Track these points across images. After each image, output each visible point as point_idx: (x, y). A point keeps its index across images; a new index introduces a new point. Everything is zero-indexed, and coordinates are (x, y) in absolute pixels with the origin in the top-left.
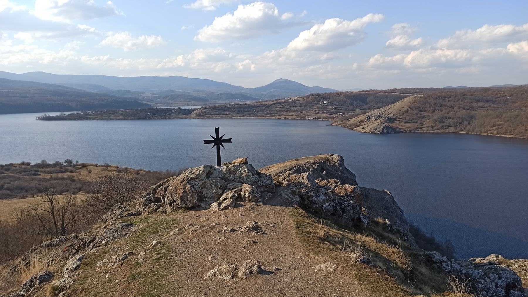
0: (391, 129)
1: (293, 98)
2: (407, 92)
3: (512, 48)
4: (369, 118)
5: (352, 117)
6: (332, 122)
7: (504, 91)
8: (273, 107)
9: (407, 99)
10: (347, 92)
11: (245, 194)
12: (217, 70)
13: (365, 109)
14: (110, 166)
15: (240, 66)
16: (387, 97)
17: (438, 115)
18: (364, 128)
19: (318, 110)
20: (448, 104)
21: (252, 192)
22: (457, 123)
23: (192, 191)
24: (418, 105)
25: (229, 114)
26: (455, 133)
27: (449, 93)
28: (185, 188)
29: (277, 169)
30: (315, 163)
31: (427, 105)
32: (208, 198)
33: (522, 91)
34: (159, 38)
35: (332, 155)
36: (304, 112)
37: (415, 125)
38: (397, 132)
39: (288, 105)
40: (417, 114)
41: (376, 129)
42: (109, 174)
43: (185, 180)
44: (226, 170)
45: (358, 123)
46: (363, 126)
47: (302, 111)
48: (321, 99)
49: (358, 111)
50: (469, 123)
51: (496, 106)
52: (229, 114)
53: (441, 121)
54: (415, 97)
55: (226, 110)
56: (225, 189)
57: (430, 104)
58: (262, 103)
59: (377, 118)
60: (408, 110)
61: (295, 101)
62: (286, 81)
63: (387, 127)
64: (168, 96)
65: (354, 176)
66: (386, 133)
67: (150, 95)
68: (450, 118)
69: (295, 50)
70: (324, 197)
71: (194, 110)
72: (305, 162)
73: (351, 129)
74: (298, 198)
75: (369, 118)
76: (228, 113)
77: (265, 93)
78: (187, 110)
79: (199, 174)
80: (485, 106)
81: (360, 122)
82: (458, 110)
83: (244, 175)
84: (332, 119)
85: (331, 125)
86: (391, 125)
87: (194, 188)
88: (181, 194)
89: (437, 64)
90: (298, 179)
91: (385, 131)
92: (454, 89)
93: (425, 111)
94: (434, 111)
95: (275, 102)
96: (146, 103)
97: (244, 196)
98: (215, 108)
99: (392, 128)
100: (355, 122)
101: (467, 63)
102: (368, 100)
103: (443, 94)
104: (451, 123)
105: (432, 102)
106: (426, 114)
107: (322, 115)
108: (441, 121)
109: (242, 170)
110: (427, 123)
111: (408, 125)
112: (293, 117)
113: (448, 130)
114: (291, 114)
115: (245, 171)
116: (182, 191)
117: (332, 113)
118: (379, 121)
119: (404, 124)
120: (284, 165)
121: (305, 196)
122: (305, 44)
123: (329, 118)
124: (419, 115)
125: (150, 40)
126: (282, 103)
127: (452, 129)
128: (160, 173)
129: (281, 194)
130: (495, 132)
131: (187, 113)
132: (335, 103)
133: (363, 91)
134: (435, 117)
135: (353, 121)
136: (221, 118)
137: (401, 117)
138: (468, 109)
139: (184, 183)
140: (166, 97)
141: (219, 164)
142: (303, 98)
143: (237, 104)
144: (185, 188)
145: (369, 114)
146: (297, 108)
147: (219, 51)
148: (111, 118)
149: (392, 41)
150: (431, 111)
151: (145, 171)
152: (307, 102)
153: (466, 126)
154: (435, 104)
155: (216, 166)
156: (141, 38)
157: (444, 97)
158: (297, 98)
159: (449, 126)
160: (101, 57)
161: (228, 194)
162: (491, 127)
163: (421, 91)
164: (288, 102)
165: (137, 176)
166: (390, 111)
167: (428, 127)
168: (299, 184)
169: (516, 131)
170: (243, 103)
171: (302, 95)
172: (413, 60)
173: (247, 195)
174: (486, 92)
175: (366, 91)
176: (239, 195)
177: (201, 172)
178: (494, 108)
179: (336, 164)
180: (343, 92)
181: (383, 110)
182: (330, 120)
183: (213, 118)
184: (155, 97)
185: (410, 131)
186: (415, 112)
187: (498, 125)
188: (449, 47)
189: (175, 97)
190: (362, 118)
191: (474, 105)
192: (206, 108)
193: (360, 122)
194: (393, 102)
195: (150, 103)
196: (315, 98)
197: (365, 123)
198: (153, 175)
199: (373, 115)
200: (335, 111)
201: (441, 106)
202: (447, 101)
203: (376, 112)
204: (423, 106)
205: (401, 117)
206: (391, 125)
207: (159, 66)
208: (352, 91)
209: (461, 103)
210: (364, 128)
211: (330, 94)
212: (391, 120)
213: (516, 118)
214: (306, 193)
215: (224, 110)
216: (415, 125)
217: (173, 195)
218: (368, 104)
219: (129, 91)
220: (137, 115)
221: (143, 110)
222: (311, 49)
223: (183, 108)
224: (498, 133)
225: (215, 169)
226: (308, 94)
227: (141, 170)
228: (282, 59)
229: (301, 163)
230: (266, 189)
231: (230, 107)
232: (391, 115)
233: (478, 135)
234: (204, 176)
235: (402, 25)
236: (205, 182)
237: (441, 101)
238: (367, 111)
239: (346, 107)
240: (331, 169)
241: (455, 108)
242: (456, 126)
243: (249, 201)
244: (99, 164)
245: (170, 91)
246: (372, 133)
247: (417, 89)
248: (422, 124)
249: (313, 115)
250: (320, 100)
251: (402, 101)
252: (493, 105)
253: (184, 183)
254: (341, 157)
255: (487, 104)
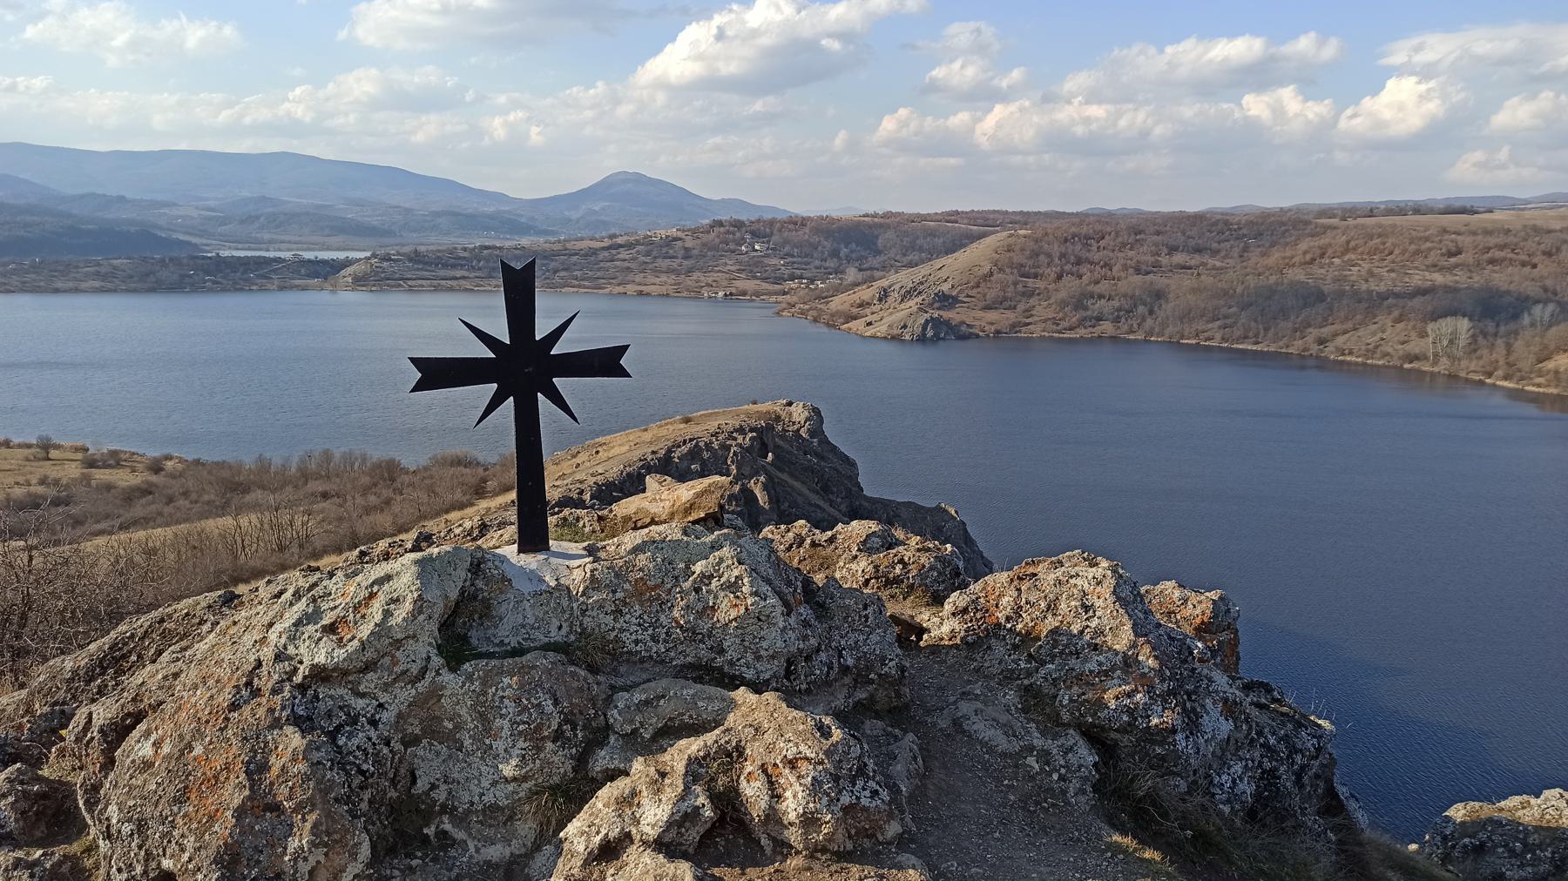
0: (945, 328)
1: (663, 233)
2: (987, 222)
3: (1255, 105)
4: (884, 295)
5: (838, 290)
6: (779, 307)
7: (1238, 223)
8: (601, 257)
9: (988, 240)
10: (821, 218)
11: (776, 796)
12: (420, 137)
13: (871, 269)
14: (57, 447)
15: (497, 127)
16: (932, 234)
17: (1070, 286)
18: (870, 324)
19: (739, 271)
20: (1097, 257)
21: (836, 777)
22: (1119, 310)
23: (324, 789)
24: (1017, 258)
25: (463, 278)
26: (1113, 338)
27: (1098, 227)
28: (256, 769)
29: (625, 448)
30: (741, 430)
31: (1042, 257)
32: (461, 820)
33: (1283, 224)
34: (228, 31)
35: (790, 404)
36: (696, 275)
37: (1011, 316)
38: (962, 334)
39: (648, 254)
40: (1015, 284)
41: (905, 327)
42: (53, 472)
43: (265, 682)
44: (594, 583)
45: (855, 310)
46: (868, 319)
47: (690, 271)
48: (748, 236)
49: (852, 274)
50: (1151, 312)
51: (1218, 264)
52: (463, 278)
53: (1079, 305)
54: (1011, 236)
55: (454, 266)
56: (599, 736)
57: (1049, 255)
58: (568, 246)
59: (907, 295)
60: (991, 274)
61: (670, 241)
62: (639, 179)
63: (936, 323)
64: (258, 217)
65: (853, 464)
66: (931, 339)
67: (195, 213)
68: (1101, 297)
69: (661, 84)
70: (1226, 727)
71: (347, 263)
72: (712, 426)
73: (834, 326)
74: (1086, 756)
75: (884, 295)
76: (459, 273)
77: (574, 215)
78: (324, 262)
79: (382, 629)
80: (1193, 263)
81: (860, 306)
82: (1123, 275)
83: (727, 611)
84: (780, 298)
85: (778, 313)
86: (946, 315)
87: (341, 760)
88: (224, 828)
89: (1058, 142)
90: (1052, 607)
91: (930, 333)
92: (1110, 214)
93: (1036, 276)
94: (1060, 277)
95: (607, 243)
96: (182, 237)
97: (773, 817)
98: (416, 258)
99: (947, 323)
100: (846, 307)
101: (1140, 143)
102: (880, 242)
103: (1084, 230)
104: (1106, 311)
105: (1056, 249)
106: (1040, 284)
107: (750, 285)
108: (1079, 305)
109: (707, 578)
110: (1042, 310)
111: (992, 315)
112: (663, 290)
113: (1098, 330)
114: (657, 280)
115: (733, 587)
116: (233, 794)
117: (778, 280)
118: (913, 304)
119: (980, 314)
120: (647, 436)
121: (1123, 730)
122: (693, 69)
123: (770, 294)
124: (1020, 287)
125: (195, 35)
126: (629, 246)
127: (1107, 327)
128: (237, 468)
129: (957, 723)
130: (1218, 336)
131: (326, 272)
132: (787, 248)
133: (866, 215)
134: (1063, 294)
135: (839, 303)
136: (437, 289)
137: (973, 292)
138: (1148, 273)
139: (254, 713)
140: (249, 219)
141: (533, 538)
142: (694, 231)
143: (487, 248)
144: (256, 769)
145: (884, 283)
146: (675, 264)
147: (426, 76)
148: (59, 285)
149: (938, 73)
150: (1053, 276)
151: (181, 460)
152: (704, 245)
153: (1144, 319)
154: (1063, 256)
155: (510, 551)
156: (169, 27)
157: (1088, 238)
158: (673, 232)
159: (1099, 319)
160: (21, 80)
161: (628, 801)
162: (1208, 322)
163: (1024, 219)
164: (647, 241)
165: (154, 478)
166: (943, 274)
167: (1045, 321)
168: (1063, 644)
169: (1270, 334)
170: (508, 244)
171: (690, 224)
172: (999, 126)
173: (793, 805)
174: (1194, 225)
175: (875, 215)
176: (728, 802)
177: (401, 614)
178: (1214, 268)
179: (803, 433)
180: (809, 218)
181: (923, 270)
182: (773, 299)
183: (411, 290)
184: (210, 219)
185: (998, 332)
186: (1011, 278)
187: (1226, 317)
188: (1093, 97)
189: (283, 220)
190: (865, 293)
191: (1164, 260)
192: (387, 258)
193: (860, 306)
194: (951, 249)
195: (194, 240)
196: (728, 232)
197: (874, 308)
198: (210, 473)
199: (897, 287)
200: (786, 272)
201: (1079, 262)
202: (1094, 248)
203: (902, 278)
204: (1030, 262)
205: (973, 292)
206: (946, 315)
207: (225, 116)
208: (834, 215)
209: (1131, 253)
210: (870, 324)
211: (772, 223)
212: (946, 301)
213: (1269, 298)
214: (1130, 712)
215: (445, 266)
216: (1011, 316)
217: (155, 831)
218: (879, 252)
219: (121, 199)
220: (152, 278)
221: (171, 260)
222: (710, 84)
223: (309, 255)
224: (1224, 339)
225: (505, 580)
226: (707, 221)
227: (169, 458)
228: (624, 110)
229: (701, 430)
230: (861, 695)
231: (466, 254)
232: (945, 287)
233: (1175, 345)
234: (424, 647)
235: (972, 25)
236: (435, 693)
237: (1078, 247)
238: (877, 274)
239: (817, 263)
240: (786, 446)
241: (1115, 269)
242: (1117, 320)
243: (815, 851)
244: (16, 440)
245: (264, 199)
246: (893, 338)
247: (1014, 213)
248: (1028, 312)
249: (725, 283)
250: (741, 242)
251: (974, 245)
252: (1211, 262)
253: (254, 713)
254: (816, 411)
255: (1195, 260)
